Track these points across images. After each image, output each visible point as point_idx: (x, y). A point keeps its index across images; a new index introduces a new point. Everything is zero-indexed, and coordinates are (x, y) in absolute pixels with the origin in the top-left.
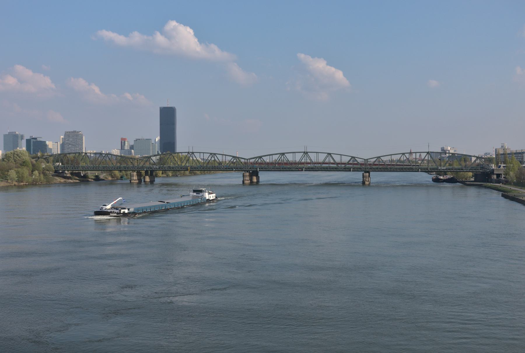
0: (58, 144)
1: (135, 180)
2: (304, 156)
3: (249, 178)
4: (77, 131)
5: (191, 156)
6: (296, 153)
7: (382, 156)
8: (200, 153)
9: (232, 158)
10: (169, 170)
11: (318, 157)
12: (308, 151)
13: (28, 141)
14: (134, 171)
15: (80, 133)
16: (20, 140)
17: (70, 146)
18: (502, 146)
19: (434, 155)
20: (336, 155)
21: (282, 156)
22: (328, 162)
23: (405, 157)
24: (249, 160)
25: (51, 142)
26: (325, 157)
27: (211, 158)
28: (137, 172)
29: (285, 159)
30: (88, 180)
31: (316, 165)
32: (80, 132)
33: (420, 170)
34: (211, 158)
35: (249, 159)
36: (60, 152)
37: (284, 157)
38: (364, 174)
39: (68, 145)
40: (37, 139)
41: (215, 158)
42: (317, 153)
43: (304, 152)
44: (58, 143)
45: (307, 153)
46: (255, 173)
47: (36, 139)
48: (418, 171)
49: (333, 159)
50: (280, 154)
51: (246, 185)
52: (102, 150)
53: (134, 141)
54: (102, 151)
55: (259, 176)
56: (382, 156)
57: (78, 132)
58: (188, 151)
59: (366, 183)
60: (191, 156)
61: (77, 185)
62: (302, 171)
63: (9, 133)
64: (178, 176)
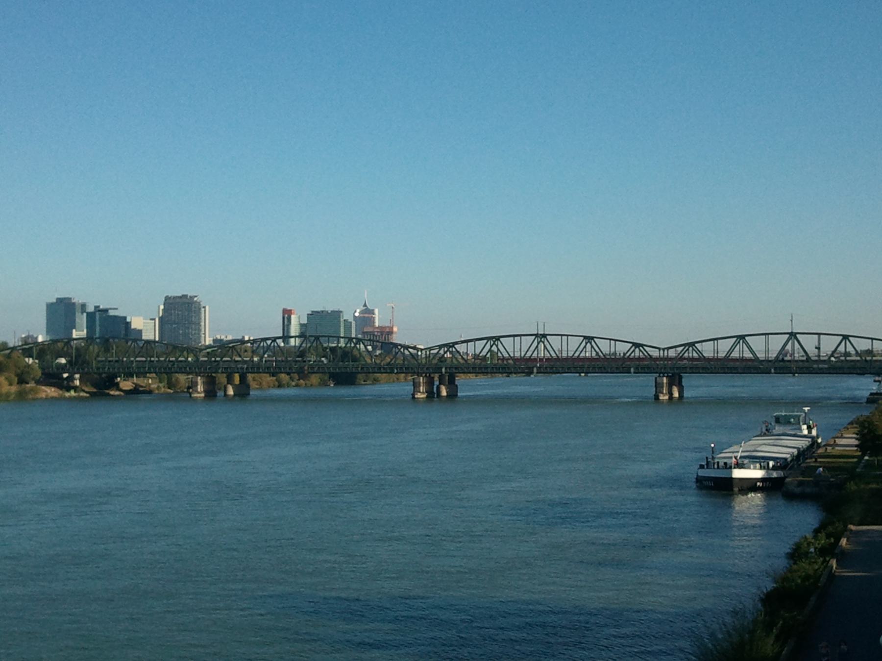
0: (155, 323)
2: (585, 347)
3: (202, 387)
4: (189, 295)
5: (494, 344)
6: (617, 342)
7: (457, 343)
8: (562, 335)
9: (631, 347)
12: (546, 333)
13: (91, 317)
15: (195, 299)
16: (80, 314)
17: (174, 326)
19: (342, 329)
22: (740, 357)
24: (666, 351)
25: (141, 318)
26: (730, 346)
27: (491, 346)
28: (208, 375)
29: (595, 350)
30: (108, 393)
32: (196, 296)
33: (773, 371)
34: (491, 346)
35: (666, 348)
36: (159, 339)
37: (592, 347)
38: (658, 379)
39: (172, 325)
40: (110, 311)
41: (499, 347)
42: (767, 336)
43: (537, 335)
44: (154, 319)
45: (544, 336)
46: (676, 379)
47: (106, 311)
48: (770, 373)
50: (488, 339)
51: (420, 401)
53: (308, 314)
54: (243, 337)
55: (456, 383)
58: (536, 333)
59: (661, 398)
60: (494, 344)
63: (58, 299)
64: (329, 385)
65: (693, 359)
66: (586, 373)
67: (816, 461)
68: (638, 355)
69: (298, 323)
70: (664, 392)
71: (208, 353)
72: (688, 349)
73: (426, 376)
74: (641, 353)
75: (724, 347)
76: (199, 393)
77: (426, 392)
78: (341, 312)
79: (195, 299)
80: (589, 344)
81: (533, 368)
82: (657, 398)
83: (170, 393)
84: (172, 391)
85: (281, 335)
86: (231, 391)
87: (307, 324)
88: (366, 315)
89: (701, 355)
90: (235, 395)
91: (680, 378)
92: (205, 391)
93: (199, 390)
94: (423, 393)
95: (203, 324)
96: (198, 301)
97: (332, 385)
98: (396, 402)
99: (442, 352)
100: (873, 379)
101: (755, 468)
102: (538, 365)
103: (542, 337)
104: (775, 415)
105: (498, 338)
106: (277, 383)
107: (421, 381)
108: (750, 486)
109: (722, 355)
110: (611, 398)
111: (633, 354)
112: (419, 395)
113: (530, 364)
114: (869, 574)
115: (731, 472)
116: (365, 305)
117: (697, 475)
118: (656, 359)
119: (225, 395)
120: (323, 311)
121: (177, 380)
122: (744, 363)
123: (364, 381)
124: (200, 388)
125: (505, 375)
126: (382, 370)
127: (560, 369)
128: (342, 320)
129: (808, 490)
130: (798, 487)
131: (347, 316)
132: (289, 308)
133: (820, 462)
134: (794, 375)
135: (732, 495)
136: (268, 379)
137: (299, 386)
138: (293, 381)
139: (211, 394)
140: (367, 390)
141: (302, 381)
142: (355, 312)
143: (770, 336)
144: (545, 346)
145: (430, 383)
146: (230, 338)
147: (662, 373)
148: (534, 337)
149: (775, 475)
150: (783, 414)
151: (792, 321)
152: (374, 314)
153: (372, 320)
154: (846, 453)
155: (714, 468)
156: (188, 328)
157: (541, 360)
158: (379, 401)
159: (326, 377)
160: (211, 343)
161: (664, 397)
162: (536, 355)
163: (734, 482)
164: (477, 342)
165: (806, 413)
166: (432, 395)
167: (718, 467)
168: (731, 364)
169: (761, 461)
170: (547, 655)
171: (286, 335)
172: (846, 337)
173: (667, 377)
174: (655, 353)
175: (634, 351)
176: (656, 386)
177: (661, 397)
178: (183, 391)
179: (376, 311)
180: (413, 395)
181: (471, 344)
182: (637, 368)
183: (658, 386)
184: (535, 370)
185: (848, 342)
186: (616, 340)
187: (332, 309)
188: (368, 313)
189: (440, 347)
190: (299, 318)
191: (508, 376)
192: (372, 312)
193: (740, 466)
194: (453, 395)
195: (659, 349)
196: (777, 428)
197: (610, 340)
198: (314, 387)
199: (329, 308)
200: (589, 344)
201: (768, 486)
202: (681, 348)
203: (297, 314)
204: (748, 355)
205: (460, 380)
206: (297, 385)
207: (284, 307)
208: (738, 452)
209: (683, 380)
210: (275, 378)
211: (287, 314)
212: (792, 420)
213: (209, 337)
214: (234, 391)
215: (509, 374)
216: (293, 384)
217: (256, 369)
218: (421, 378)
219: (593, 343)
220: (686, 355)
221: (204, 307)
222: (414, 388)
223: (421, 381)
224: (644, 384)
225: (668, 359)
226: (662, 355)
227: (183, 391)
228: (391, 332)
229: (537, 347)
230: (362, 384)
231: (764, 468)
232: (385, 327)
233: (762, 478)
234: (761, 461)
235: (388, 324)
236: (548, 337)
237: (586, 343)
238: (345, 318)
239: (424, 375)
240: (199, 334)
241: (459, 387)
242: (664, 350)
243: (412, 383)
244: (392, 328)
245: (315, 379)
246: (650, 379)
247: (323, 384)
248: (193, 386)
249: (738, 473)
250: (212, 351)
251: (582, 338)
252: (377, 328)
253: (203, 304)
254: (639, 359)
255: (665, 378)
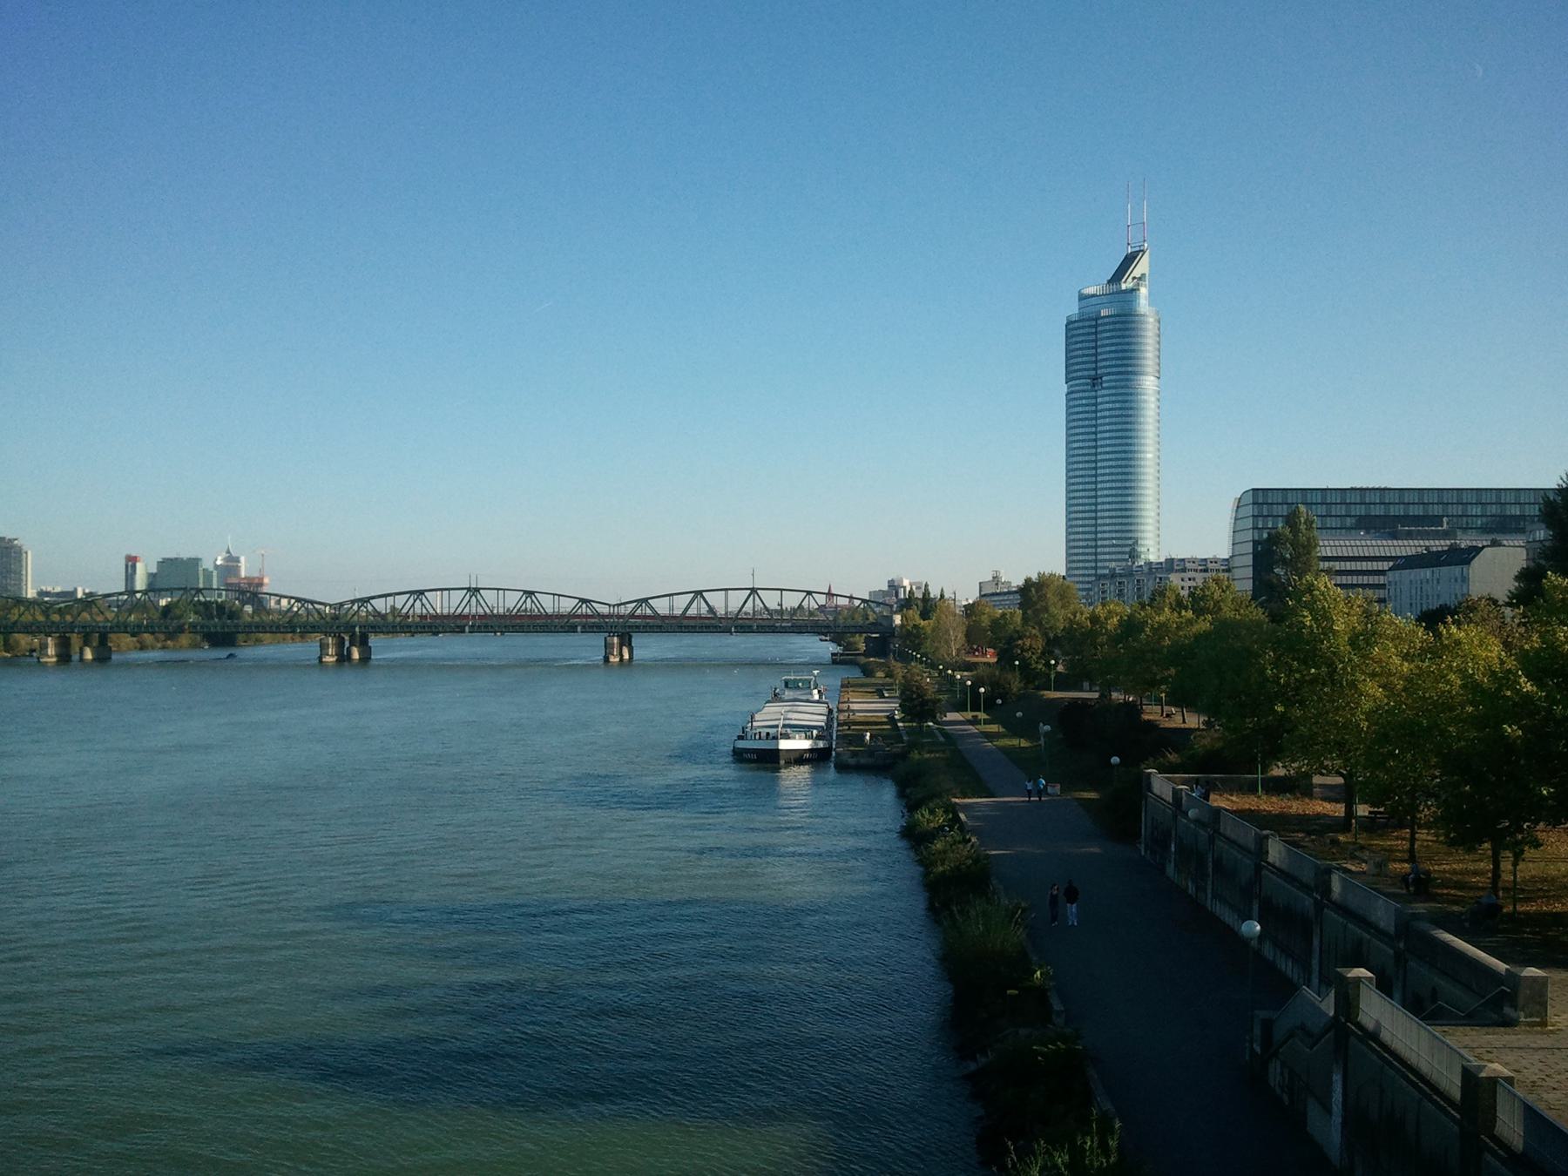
1: (52, 657)
6: (784, 592)
7: (373, 598)
8: (498, 589)
10: (420, 632)
11: (278, 602)
14: (48, 635)
15: (16, 542)
18: (994, 578)
20: (489, 591)
21: (527, 598)
23: (706, 606)
24: (616, 607)
31: (648, 621)
32: (16, 539)
33: (733, 630)
37: (532, 601)
38: (608, 638)
43: (469, 589)
45: (477, 590)
46: (626, 640)
49: (652, 608)
50: (411, 593)
52: (75, 586)
55: (370, 644)
56: (373, 598)
57: (10, 540)
58: (468, 586)
60: (473, 594)
61: (434, 659)
62: (463, 634)
65: (645, 617)
66: (503, 633)
67: (849, 729)
68: (420, 611)
69: (144, 572)
70: (615, 653)
71: (60, 608)
72: (641, 605)
73: (335, 636)
74: (424, 609)
75: (680, 604)
76: (49, 657)
77: (336, 655)
78: (201, 559)
79: (16, 542)
80: (529, 599)
81: (465, 626)
82: (606, 659)
83: (5, 658)
84: (9, 655)
85: (123, 590)
86: (88, 655)
87: (156, 574)
88: (231, 564)
89: (542, 611)
90: (94, 659)
91: (630, 637)
92: (57, 655)
93: (49, 653)
94: (332, 656)
95: (24, 573)
96: (19, 545)
97: (207, 647)
98: (298, 666)
99: (355, 607)
100: (817, 638)
101: (800, 739)
102: (471, 623)
103: (474, 591)
104: (784, 678)
105: (421, 592)
106: (138, 645)
107: (330, 641)
108: (798, 758)
109: (678, 612)
110: (555, 660)
111: (580, 611)
112: (327, 659)
113: (459, 622)
114: (1008, 852)
115: (778, 744)
116: (228, 552)
117: (734, 747)
118: (603, 616)
119: (81, 659)
120: (176, 559)
121: (17, 643)
122: (702, 621)
123: (245, 642)
124: (51, 651)
125: (408, 634)
126: (115, 629)
127: (553, 628)
128: (200, 569)
129: (863, 761)
130: (852, 758)
131: (207, 564)
132: (134, 554)
133: (853, 729)
134: (495, 634)
135: (778, 770)
136: (127, 640)
137: (167, 648)
138: (158, 642)
139: (64, 658)
140: (247, 652)
141: (169, 642)
142: (216, 560)
143: (729, 592)
144: (477, 600)
145: (340, 644)
146: (58, 589)
147: (611, 633)
148: (465, 591)
149: (821, 744)
150: (792, 678)
151: (753, 575)
152: (239, 562)
153: (237, 569)
154: (871, 720)
155: (755, 739)
156: (5, 577)
157: (474, 617)
158: (260, 665)
159: (199, 638)
160: (35, 595)
161: (614, 659)
162: (468, 611)
163: (781, 754)
164: (397, 597)
165: (815, 677)
166: (343, 658)
167: (760, 738)
168: (686, 622)
169: (805, 730)
170: (48, 876)
171: (129, 589)
172: (809, 593)
173: (617, 636)
174: (604, 610)
175: (581, 606)
176: (605, 646)
177: (612, 659)
178: (24, 655)
179: (242, 559)
180: (320, 658)
181: (390, 599)
182: (584, 627)
183: (608, 647)
184: (467, 629)
185: (756, 596)
186: (559, 595)
187: (189, 557)
188: (232, 563)
189: (353, 602)
190: (146, 566)
191: (413, 636)
192: (237, 560)
193: (786, 737)
194: (365, 659)
195: (609, 605)
196: (786, 693)
197: (554, 595)
198: (185, 649)
199: (185, 555)
200: (529, 599)
201: (815, 758)
202: (635, 604)
203: (144, 561)
204: (704, 610)
205: (374, 641)
206: (164, 648)
207: (129, 553)
208: (780, 719)
209: (633, 640)
210: (135, 639)
211: (131, 562)
212: (800, 684)
213: (32, 589)
214: (93, 655)
215: (436, 634)
216: (159, 645)
217: (122, 628)
218: (330, 638)
219: (533, 597)
220: (639, 611)
221: (26, 553)
222: (321, 651)
223: (330, 641)
224: (589, 647)
225: (619, 616)
226: (612, 611)
227: (24, 655)
228: (261, 584)
229: (469, 601)
230: (242, 646)
231: (809, 739)
232: (254, 578)
233: (809, 750)
234: (805, 730)
235: (256, 574)
236: (481, 591)
237: (527, 598)
238: (204, 567)
239: (333, 635)
240: (20, 584)
241: (372, 649)
242: (614, 606)
243: (318, 644)
244: (262, 579)
245: (184, 639)
246: (598, 640)
247: (195, 646)
248: (44, 647)
249: (784, 745)
250: (66, 606)
251: (522, 593)
252: (245, 578)
253: (24, 548)
254: (587, 616)
255: (616, 638)
